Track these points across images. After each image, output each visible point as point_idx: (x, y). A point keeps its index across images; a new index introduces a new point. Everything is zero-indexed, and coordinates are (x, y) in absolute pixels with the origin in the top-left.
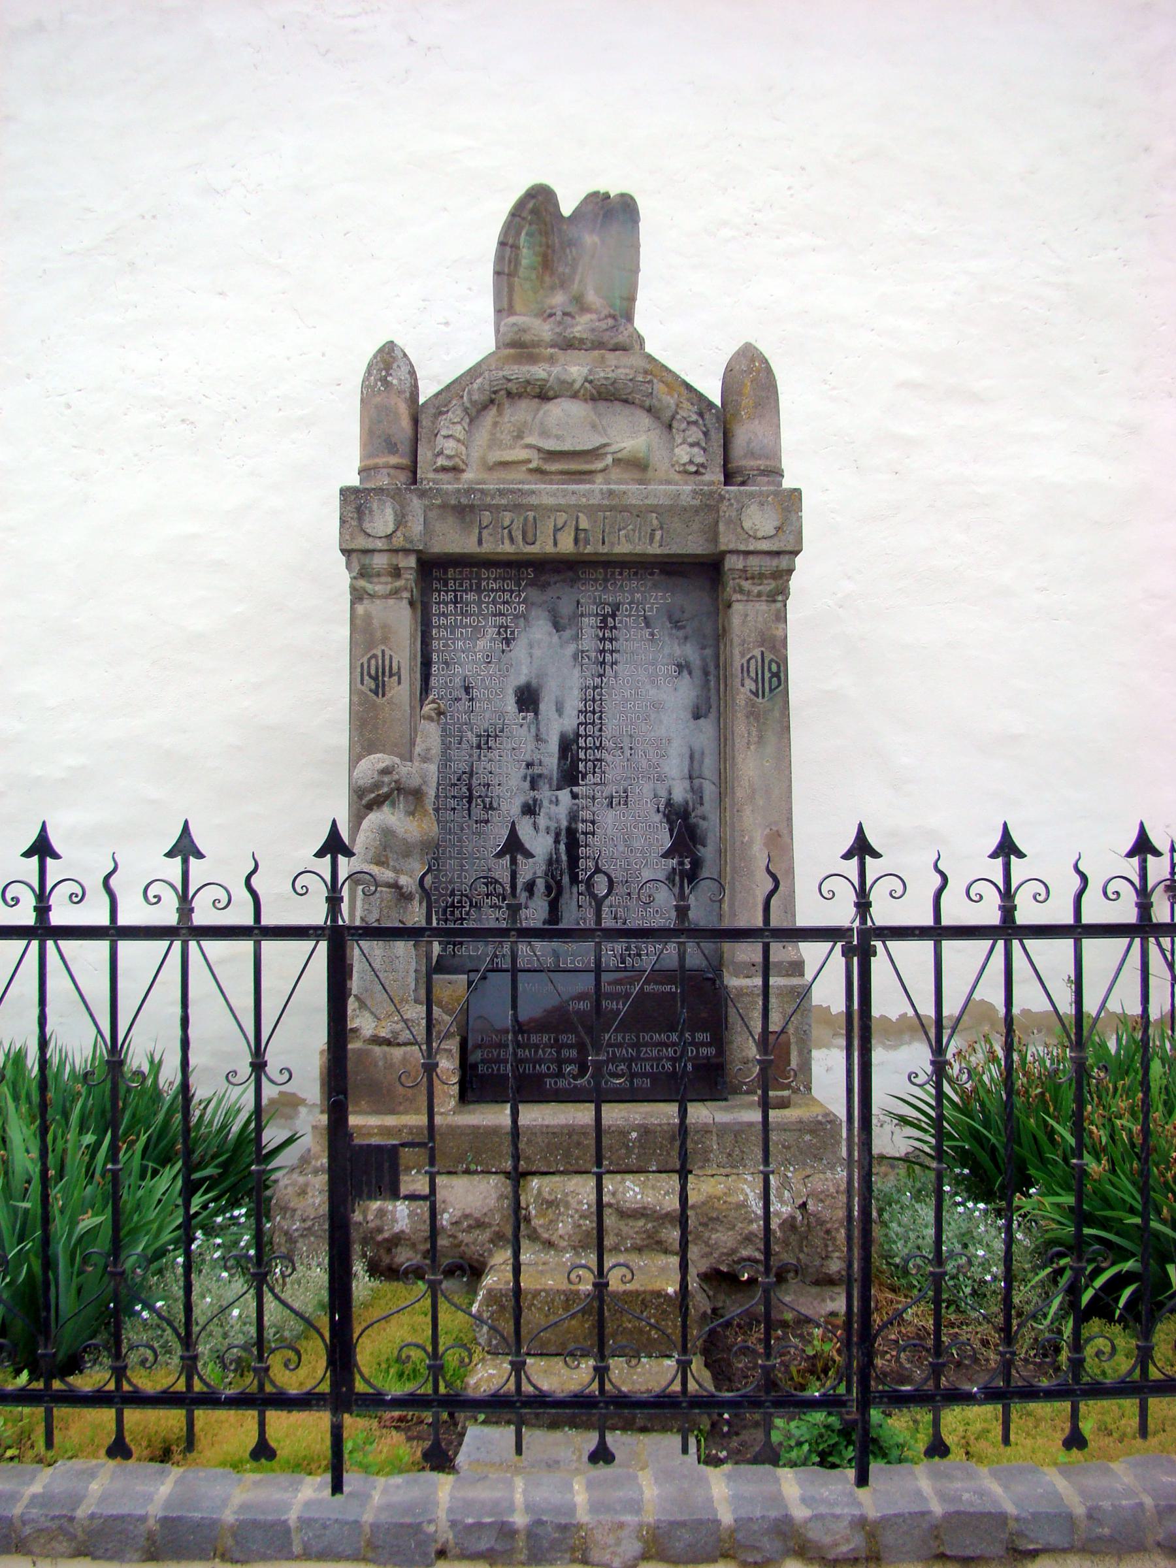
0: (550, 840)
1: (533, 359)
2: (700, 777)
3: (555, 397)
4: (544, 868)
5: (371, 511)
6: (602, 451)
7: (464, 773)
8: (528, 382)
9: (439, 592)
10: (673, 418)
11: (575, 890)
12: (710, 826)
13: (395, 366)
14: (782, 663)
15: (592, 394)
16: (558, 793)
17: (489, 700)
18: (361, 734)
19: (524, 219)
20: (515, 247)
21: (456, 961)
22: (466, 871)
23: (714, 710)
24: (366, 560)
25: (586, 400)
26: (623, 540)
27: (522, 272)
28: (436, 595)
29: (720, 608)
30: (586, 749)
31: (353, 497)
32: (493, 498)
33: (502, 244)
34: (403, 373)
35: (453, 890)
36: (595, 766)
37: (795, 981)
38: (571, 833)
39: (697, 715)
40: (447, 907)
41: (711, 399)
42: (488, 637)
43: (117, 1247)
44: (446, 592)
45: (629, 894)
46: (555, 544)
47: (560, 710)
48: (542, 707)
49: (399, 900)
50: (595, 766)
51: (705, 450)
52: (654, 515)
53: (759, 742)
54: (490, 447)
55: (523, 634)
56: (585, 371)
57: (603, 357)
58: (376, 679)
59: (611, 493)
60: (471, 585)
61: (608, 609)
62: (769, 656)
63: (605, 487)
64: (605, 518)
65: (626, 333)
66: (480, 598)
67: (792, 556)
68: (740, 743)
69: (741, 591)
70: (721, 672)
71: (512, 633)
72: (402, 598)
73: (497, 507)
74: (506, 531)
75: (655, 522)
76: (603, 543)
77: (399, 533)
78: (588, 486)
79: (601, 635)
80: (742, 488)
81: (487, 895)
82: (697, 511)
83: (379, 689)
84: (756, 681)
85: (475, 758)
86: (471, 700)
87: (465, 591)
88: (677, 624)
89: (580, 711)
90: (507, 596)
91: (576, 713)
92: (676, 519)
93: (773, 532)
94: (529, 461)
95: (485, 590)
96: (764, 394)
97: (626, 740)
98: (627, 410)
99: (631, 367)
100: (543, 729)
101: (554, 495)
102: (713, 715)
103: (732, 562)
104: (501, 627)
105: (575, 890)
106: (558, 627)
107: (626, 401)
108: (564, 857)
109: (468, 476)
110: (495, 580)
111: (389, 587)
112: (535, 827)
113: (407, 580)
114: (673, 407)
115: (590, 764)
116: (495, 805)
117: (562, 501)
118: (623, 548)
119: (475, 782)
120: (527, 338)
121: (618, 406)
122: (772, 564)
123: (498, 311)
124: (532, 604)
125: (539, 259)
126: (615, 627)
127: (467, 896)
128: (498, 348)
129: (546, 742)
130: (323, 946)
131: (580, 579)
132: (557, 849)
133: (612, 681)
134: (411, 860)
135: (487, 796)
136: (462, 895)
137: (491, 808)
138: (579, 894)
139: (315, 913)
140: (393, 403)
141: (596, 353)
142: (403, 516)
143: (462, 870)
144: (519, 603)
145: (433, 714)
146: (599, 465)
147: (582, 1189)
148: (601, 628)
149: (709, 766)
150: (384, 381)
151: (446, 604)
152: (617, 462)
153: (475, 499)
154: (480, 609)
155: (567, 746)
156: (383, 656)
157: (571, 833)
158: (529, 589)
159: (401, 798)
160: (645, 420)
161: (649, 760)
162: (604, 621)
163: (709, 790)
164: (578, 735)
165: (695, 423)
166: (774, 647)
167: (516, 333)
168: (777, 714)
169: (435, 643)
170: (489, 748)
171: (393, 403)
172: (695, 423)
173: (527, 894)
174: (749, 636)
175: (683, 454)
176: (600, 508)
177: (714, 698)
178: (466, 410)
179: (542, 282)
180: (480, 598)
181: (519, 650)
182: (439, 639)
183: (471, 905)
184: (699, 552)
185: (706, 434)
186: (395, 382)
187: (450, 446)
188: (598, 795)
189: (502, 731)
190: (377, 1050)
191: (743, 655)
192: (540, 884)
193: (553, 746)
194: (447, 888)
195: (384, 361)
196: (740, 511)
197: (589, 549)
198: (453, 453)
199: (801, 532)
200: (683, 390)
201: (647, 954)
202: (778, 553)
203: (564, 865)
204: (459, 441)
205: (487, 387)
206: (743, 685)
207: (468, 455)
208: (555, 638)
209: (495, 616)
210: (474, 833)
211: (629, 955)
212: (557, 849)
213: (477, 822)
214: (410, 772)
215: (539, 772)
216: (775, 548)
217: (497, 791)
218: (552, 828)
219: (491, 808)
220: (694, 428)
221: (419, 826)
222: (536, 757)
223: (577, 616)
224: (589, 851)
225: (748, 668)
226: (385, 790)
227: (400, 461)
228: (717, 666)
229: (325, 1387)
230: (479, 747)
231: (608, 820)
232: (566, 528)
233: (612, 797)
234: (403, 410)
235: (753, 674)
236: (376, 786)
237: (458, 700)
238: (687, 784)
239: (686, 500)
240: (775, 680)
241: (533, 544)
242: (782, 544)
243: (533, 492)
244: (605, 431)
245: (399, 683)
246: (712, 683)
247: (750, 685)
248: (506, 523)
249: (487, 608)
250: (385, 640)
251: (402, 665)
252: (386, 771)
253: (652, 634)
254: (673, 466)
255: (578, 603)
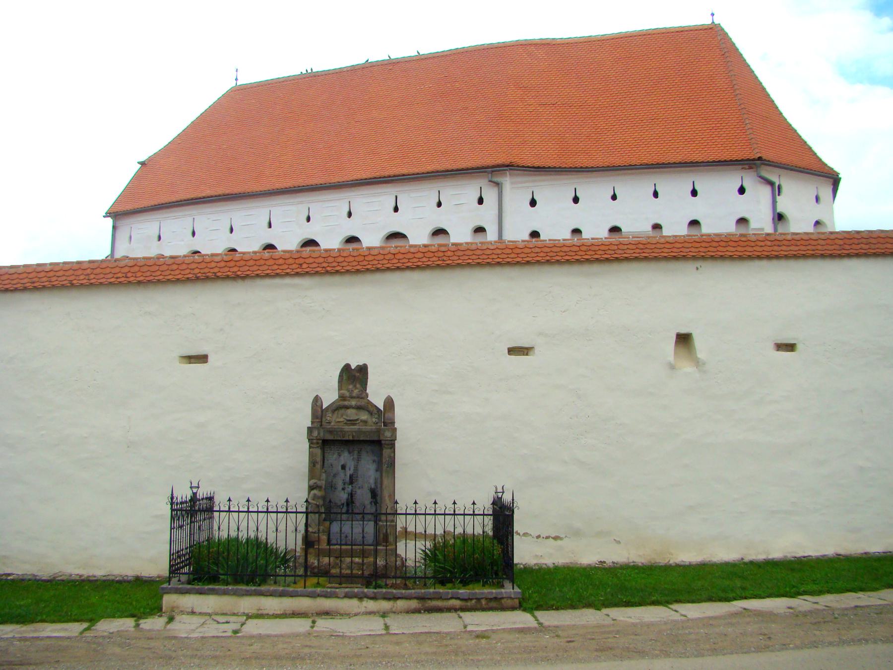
0: (347, 495)
12: (379, 493)
20: (342, 376)
29: (381, 450)
33: (340, 376)
38: (351, 494)
39: (377, 471)
43: (266, 566)
47: (350, 470)
83: (314, 466)
106: (350, 453)
112: (344, 492)
118: (362, 439)
122: (391, 442)
128: (339, 397)
130: (305, 514)
139: (304, 510)
146: (358, 422)
147: (348, 560)
149: (379, 481)
152: (361, 421)
155: (351, 476)
157: (351, 494)
160: (367, 413)
163: (379, 486)
175: (374, 420)
181: (342, 458)
187: (328, 418)
190: (312, 534)
192: (345, 504)
193: (348, 477)
202: (392, 440)
208: (349, 455)
214: (319, 483)
223: (353, 451)
229: (304, 574)
231: (359, 491)
234: (320, 410)
236: (313, 486)
247: (386, 466)
252: (315, 483)
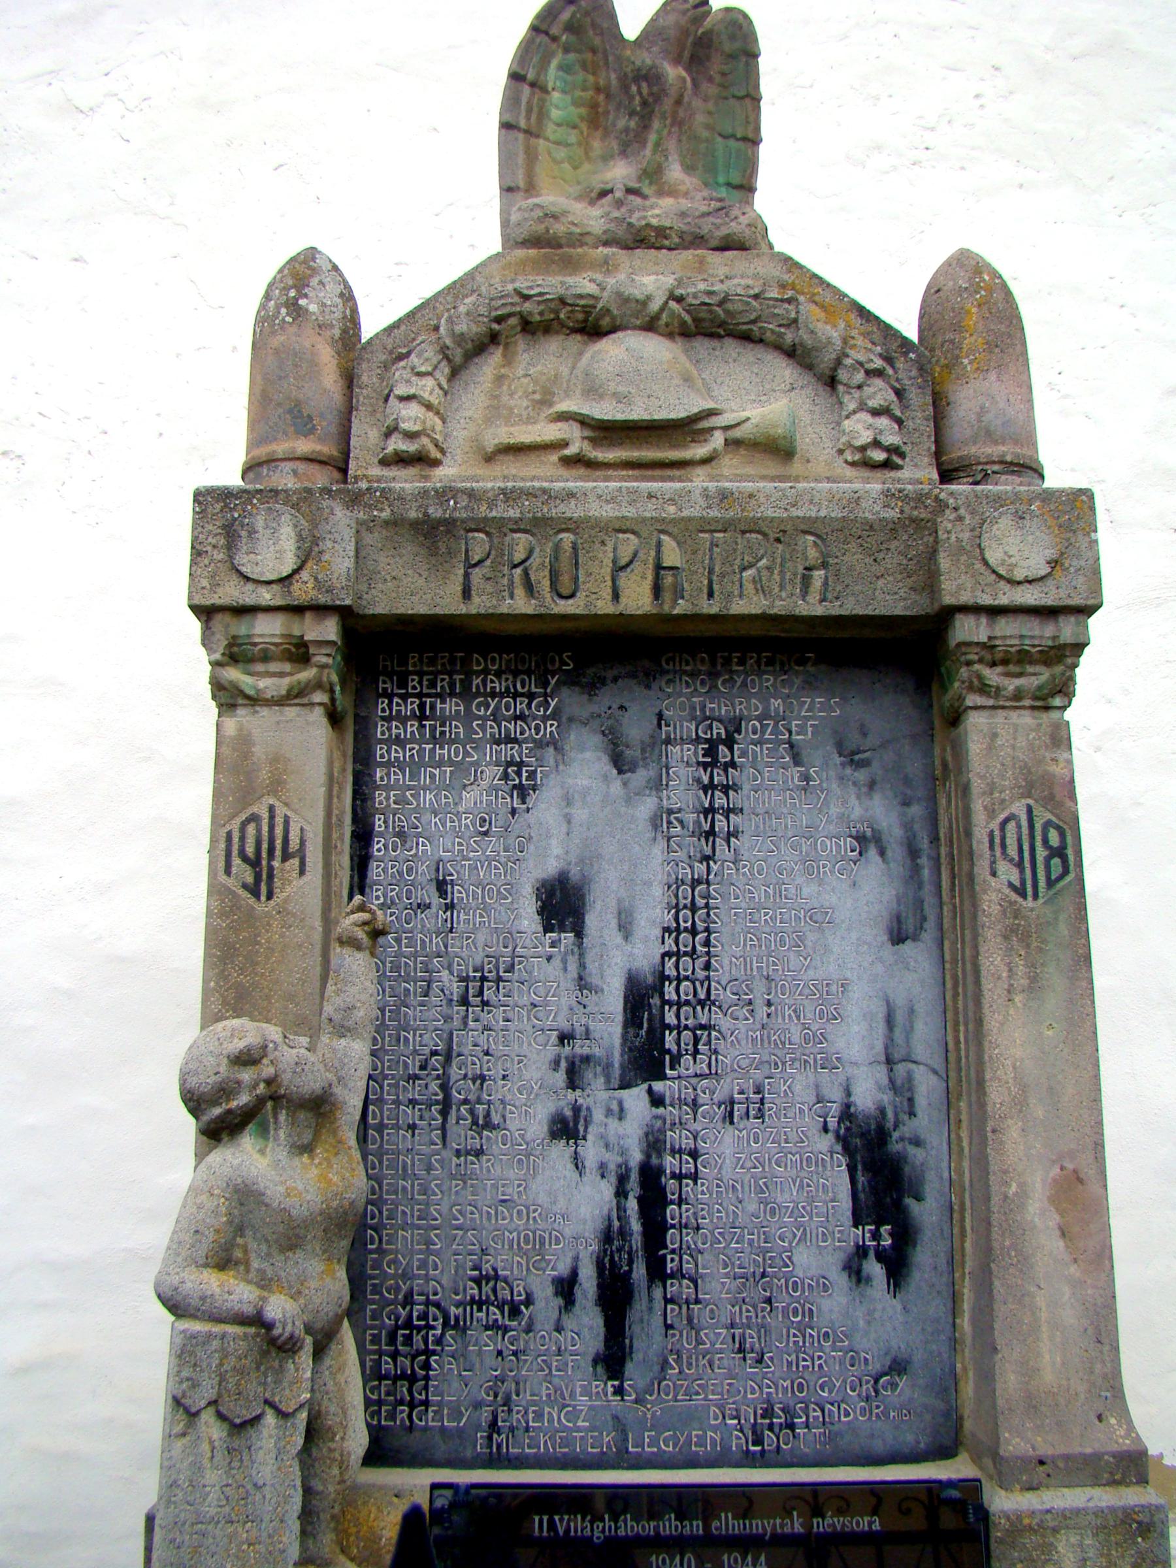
0: (607, 1190)
1: (571, 265)
2: (908, 1059)
3: (613, 330)
4: (595, 1247)
5: (252, 532)
6: (705, 424)
7: (434, 1053)
8: (562, 301)
9: (390, 697)
10: (838, 362)
11: (658, 1293)
13: (314, 282)
14: (1068, 827)
15: (683, 323)
16: (624, 1094)
17: (486, 908)
18: (223, 976)
19: (554, 39)
21: (414, 1441)
22: (437, 1253)
23: (930, 924)
24: (241, 628)
25: (670, 336)
26: (749, 588)
27: (550, 130)
28: (383, 703)
30: (680, 1004)
31: (218, 506)
32: (492, 505)
33: (515, 77)
34: (330, 294)
35: (410, 1293)
36: (696, 1040)
37: (1131, 1496)
38: (650, 1175)
40: (397, 1327)
41: (905, 334)
42: (484, 784)
44: (404, 697)
45: (769, 1301)
46: (616, 596)
47: (625, 928)
48: (591, 921)
49: (265, 1354)
50: (696, 1040)
51: (899, 422)
52: (811, 538)
53: (1030, 988)
54: (488, 421)
55: (553, 780)
56: (669, 281)
57: (702, 261)
58: (255, 863)
59: (724, 496)
60: (452, 685)
61: (719, 730)
62: (1042, 816)
63: (712, 485)
64: (714, 545)
65: (744, 220)
66: (468, 709)
67: (1081, 618)
68: (992, 991)
69: (983, 689)
70: (943, 850)
71: (532, 775)
72: (312, 704)
73: (501, 522)
74: (518, 571)
75: (812, 553)
76: (711, 595)
77: (305, 575)
78: (678, 485)
79: (706, 780)
80: (979, 488)
81: (480, 1304)
82: (893, 529)
84: (1020, 865)
85: (457, 1023)
86: (450, 907)
87: (441, 697)
88: (853, 758)
89: (666, 930)
90: (521, 705)
91: (658, 932)
92: (853, 546)
93: (1044, 570)
94: (565, 444)
95: (478, 694)
96: (1003, 328)
97: (760, 987)
98: (750, 353)
99: (756, 276)
100: (592, 967)
101: (613, 500)
102: (929, 936)
103: (967, 630)
104: (509, 764)
105: (658, 1293)
106: (620, 763)
107: (746, 337)
108: (636, 1226)
109: (446, 473)
110: (498, 674)
111: (286, 681)
112: (578, 1163)
113: (323, 667)
114: (838, 343)
115: (687, 1035)
116: (496, 1119)
117: (630, 512)
119: (455, 1072)
120: (559, 228)
121: (731, 347)
123: (508, 190)
124: (571, 720)
125: (583, 111)
126: (733, 764)
127: (437, 1305)
129: (597, 990)
131: (664, 672)
132: (621, 1209)
133: (729, 871)
134: (299, 1254)
135: (479, 1101)
136: (428, 1303)
137: (489, 1125)
138: (667, 1301)
140: (307, 344)
141: (688, 255)
142: (316, 541)
143: (429, 1252)
144: (545, 719)
145: (361, 934)
146: (699, 451)
148: (705, 765)
150: (294, 307)
151: (403, 720)
152: (734, 444)
153: (459, 509)
154: (470, 730)
156: (272, 817)
157: (650, 1175)
158: (565, 692)
159: (282, 1117)
160: (784, 371)
161: (805, 1027)
162: (711, 752)
163: (927, 1086)
164: (663, 978)
165: (879, 373)
166: (1052, 797)
167: (540, 220)
168: (1063, 929)
169: (380, 796)
170: (485, 1003)
171: (307, 344)
172: (879, 373)
173: (560, 1301)
174: (1003, 777)
175: (861, 428)
176: (705, 526)
177: (929, 901)
178: (443, 350)
179: (587, 149)
180: (468, 709)
182: (388, 788)
183: (446, 1324)
184: (898, 612)
185: (899, 393)
186: (313, 308)
187: (411, 416)
188: (703, 1098)
189: (510, 969)
191: (991, 813)
193: (613, 1000)
194: (398, 1289)
195: (295, 275)
196: (977, 533)
197: (682, 607)
198: (417, 428)
199: (1096, 572)
200: (856, 321)
201: (807, 1425)
203: (637, 1241)
204: (429, 406)
205: (483, 310)
206: (994, 874)
207: (446, 436)
208: (616, 787)
209: (498, 742)
210: (452, 1177)
211: (771, 1427)
212: (621, 1209)
213: (458, 1153)
215: (586, 1051)
216: (1049, 601)
217: (498, 1091)
218: (612, 1166)
219: (489, 1125)
220: (878, 382)
221: (322, 1177)
222: (579, 1022)
223: (658, 743)
224: (687, 1213)
225: (1003, 838)
226: (243, 1099)
227: (318, 448)
228: (935, 839)
230: (464, 1001)
232: (635, 564)
233: (732, 1102)
234: (327, 358)
235: (1012, 851)
237: (424, 907)
238: (881, 1073)
239: (872, 509)
240: (1056, 862)
241: (572, 596)
242: (1063, 593)
243: (571, 495)
244: (709, 390)
245: (302, 872)
246: (926, 872)
247: (1008, 872)
248: (519, 556)
249: (482, 727)
250: (276, 786)
251: (309, 835)
252: (246, 1059)
253: (806, 778)
254: (841, 452)
255: (660, 716)
